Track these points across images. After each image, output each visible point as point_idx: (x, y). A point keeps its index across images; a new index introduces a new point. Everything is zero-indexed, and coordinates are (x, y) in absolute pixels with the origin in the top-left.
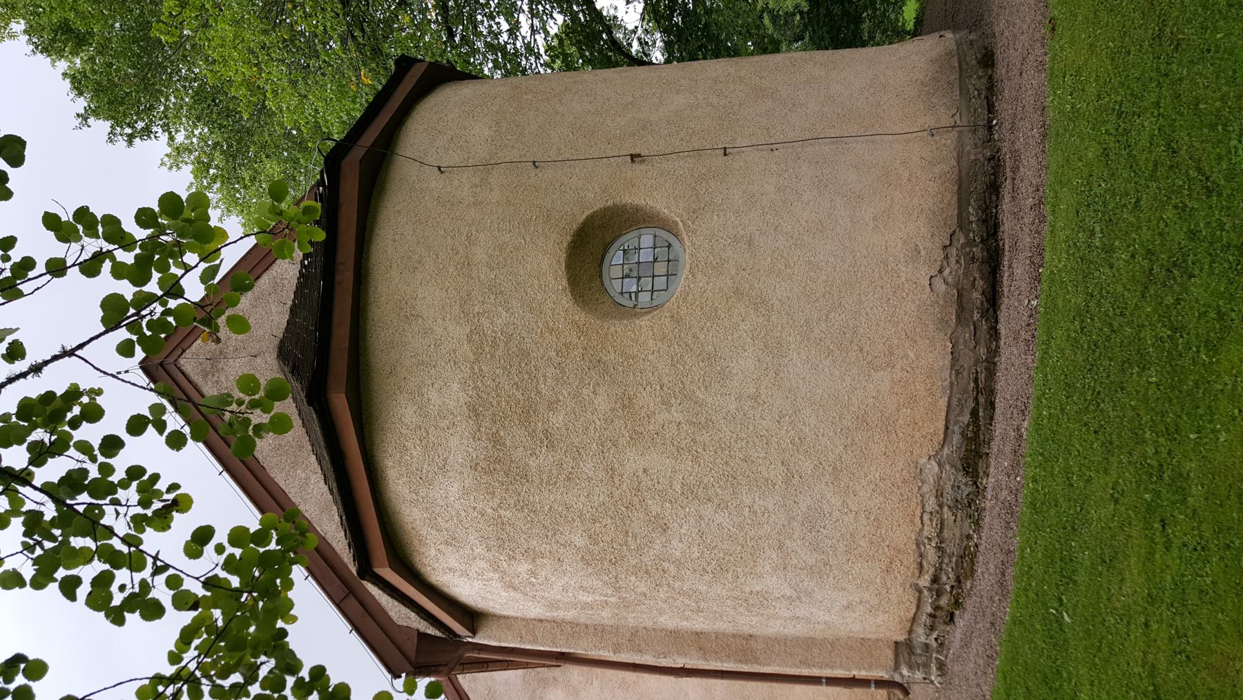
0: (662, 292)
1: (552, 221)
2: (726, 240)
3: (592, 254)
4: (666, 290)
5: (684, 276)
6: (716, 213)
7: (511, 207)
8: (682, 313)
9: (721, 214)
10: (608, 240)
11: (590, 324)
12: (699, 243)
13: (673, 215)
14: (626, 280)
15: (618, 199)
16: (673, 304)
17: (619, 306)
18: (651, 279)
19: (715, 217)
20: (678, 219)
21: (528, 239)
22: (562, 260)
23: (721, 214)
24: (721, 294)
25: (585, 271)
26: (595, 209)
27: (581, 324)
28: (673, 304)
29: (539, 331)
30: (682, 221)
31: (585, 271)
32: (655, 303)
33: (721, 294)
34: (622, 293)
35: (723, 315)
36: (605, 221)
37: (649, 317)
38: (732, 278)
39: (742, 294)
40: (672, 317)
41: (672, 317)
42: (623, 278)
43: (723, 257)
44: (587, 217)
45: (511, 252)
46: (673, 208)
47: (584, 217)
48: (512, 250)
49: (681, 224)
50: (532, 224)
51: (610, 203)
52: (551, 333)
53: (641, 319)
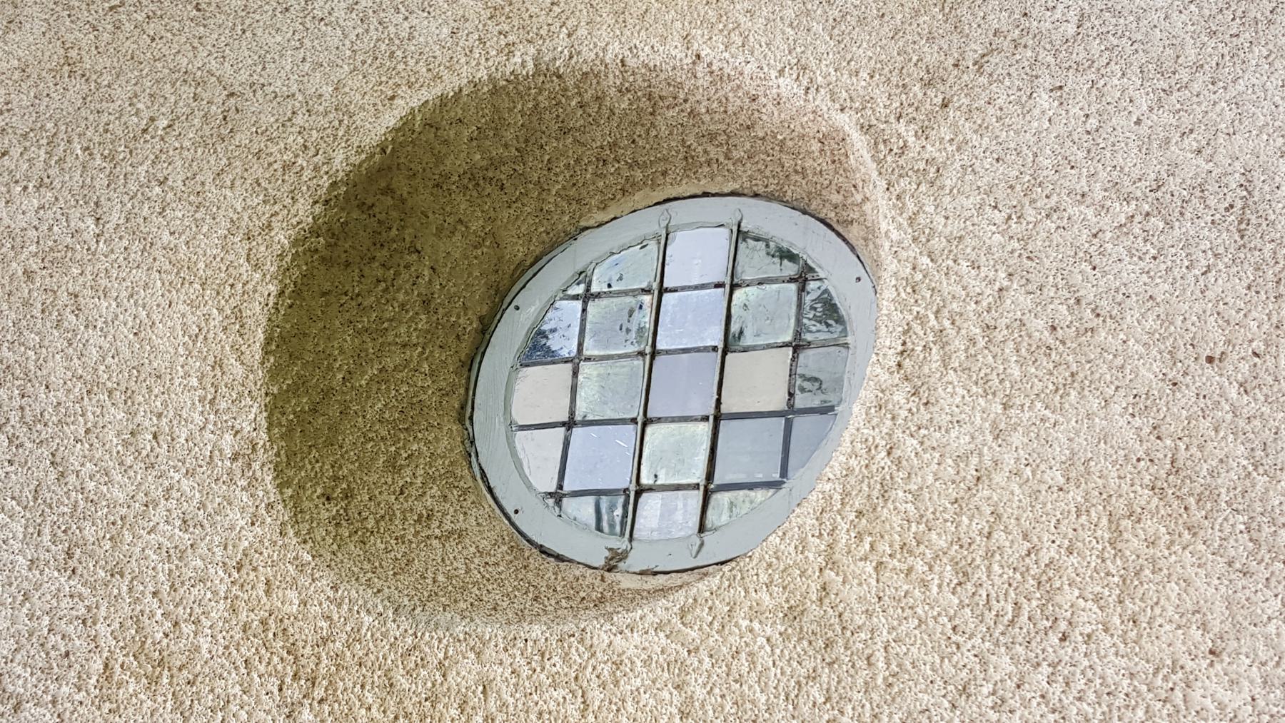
0: (759, 495)
1: (240, 138)
2: (1103, 208)
3: (426, 303)
4: (774, 485)
5: (867, 394)
6: (1046, 81)
7: (79, 86)
8: (851, 593)
9: (1077, 83)
10: (518, 250)
11: (355, 637)
12: (955, 227)
13: (821, 101)
14: (623, 479)
15: (562, 41)
16: (803, 547)
17: (536, 560)
18: (705, 429)
19: (1044, 100)
20: (846, 122)
21: (116, 217)
22: (257, 313)
23: (1077, 83)
24: (1075, 495)
25: (383, 377)
26: (449, 84)
27: (305, 633)
28: (803, 547)
29: (97, 666)
30: (866, 129)
31: (383, 377)
32: (716, 547)
33: (1075, 495)
34: (558, 496)
35: (1089, 617)
36: (499, 151)
37: (662, 609)
38: (1141, 404)
39: (1208, 496)
40: (793, 614)
41: (793, 614)
42: (570, 424)
43: (1088, 293)
44: (406, 125)
45: (28, 274)
46: (822, 72)
47: (390, 119)
48: (34, 265)
49: (859, 143)
50: (147, 149)
51: (522, 60)
52: (154, 680)
53: (622, 619)
